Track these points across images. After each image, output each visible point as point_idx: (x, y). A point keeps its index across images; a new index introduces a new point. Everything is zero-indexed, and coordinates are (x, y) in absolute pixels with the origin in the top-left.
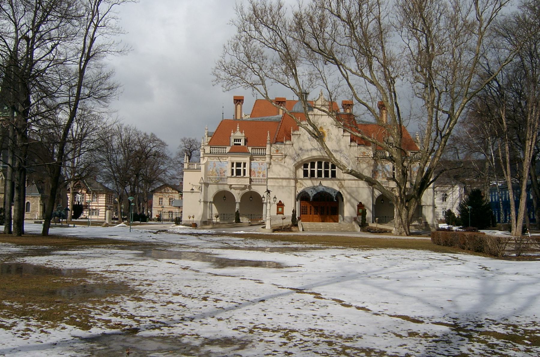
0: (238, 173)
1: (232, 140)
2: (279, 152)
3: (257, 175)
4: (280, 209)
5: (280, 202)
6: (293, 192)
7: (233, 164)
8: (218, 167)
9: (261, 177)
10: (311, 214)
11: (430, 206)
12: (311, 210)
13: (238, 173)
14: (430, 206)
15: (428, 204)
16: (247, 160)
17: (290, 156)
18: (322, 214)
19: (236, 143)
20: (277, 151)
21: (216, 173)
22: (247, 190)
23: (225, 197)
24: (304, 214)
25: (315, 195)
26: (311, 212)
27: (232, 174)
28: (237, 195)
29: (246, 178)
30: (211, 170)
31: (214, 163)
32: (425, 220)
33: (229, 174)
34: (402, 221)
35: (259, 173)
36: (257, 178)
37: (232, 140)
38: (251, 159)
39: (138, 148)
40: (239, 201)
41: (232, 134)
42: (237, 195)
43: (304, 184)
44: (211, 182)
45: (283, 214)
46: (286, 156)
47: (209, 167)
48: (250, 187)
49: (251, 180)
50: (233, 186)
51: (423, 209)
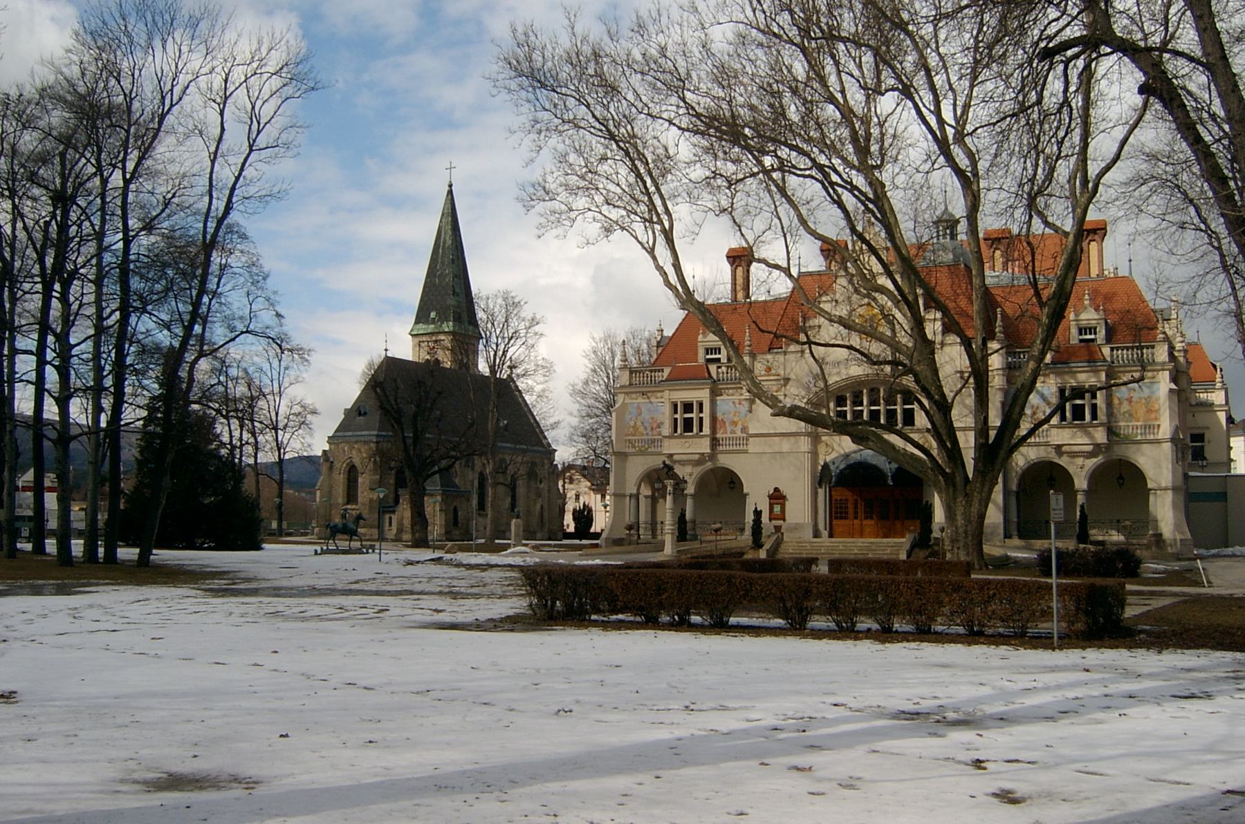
0: (688, 425)
1: (701, 352)
2: (773, 371)
3: (729, 429)
4: (777, 509)
5: (776, 490)
6: (808, 465)
7: (675, 406)
8: (646, 416)
9: (739, 434)
10: (856, 518)
11: (1166, 489)
12: (856, 507)
13: (688, 425)
14: (1166, 489)
15: (1163, 485)
16: (703, 395)
17: (798, 380)
18: (883, 517)
19: (709, 357)
20: (769, 369)
21: (641, 429)
22: (709, 465)
23: (1121, 477)
24: (841, 518)
25: (841, 471)
26: (856, 513)
27: (676, 431)
28: (1081, 472)
29: (703, 436)
30: (632, 423)
31: (639, 408)
32: (1156, 527)
33: (666, 430)
34: (957, 533)
35: (735, 423)
36: (729, 435)
37: (701, 352)
38: (715, 393)
39: (241, 390)
40: (1085, 486)
41: (700, 338)
42: (1081, 472)
43: (836, 447)
44: (631, 450)
45: (784, 520)
46: (787, 380)
47: (628, 417)
48: (713, 456)
49: (715, 442)
50: (1064, 449)
51: (1151, 498)
